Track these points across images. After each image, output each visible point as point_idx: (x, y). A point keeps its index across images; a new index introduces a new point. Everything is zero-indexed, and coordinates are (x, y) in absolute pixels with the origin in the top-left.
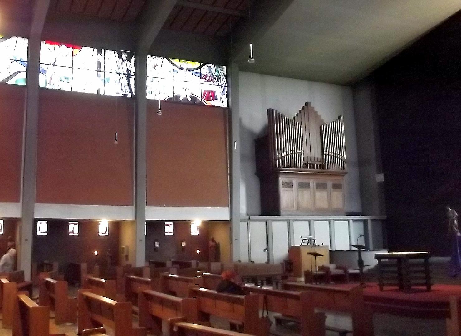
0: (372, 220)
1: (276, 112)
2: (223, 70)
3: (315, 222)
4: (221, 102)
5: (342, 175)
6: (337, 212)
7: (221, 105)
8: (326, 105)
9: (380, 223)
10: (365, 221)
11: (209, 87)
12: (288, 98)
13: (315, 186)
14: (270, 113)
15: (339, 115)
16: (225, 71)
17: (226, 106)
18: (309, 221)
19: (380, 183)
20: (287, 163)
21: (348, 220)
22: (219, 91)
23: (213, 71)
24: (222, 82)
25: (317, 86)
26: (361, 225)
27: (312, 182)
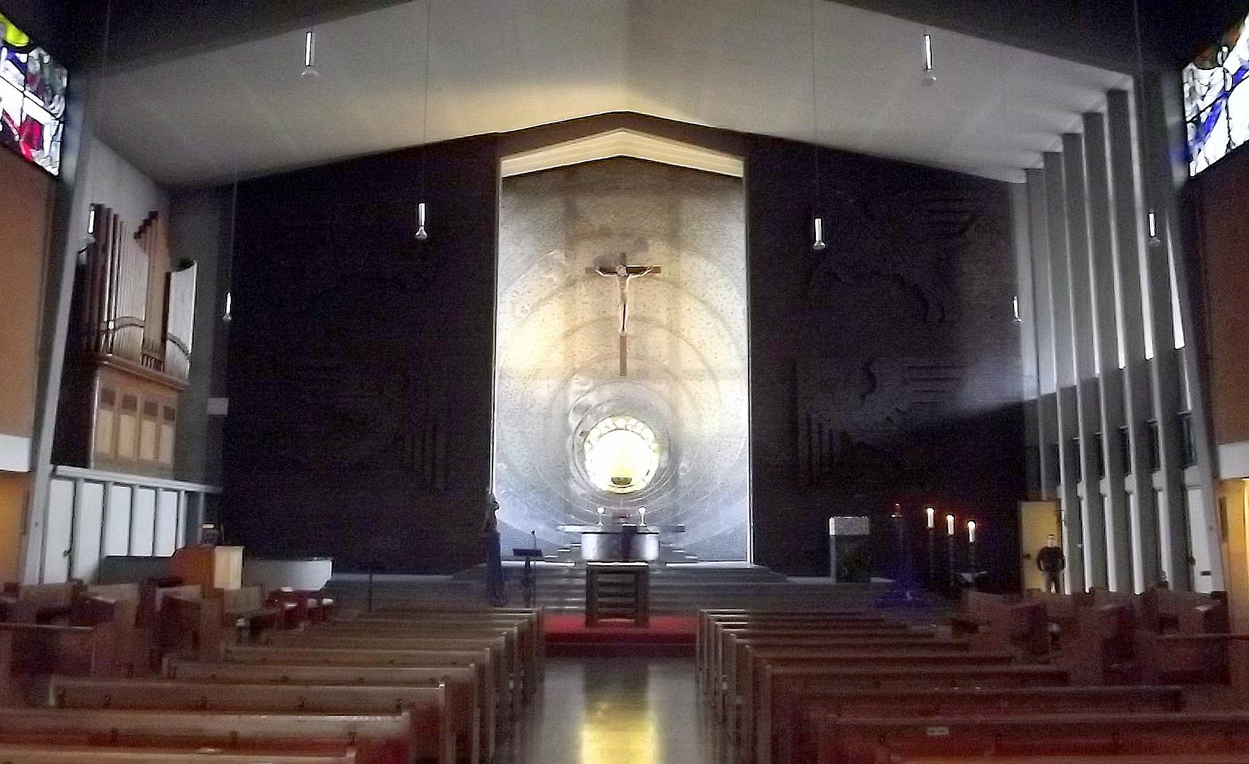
0: (207, 495)
1: (116, 217)
6: (160, 472)
7: (49, 169)
17: (55, 172)
19: (214, 418)
23: (47, 72)
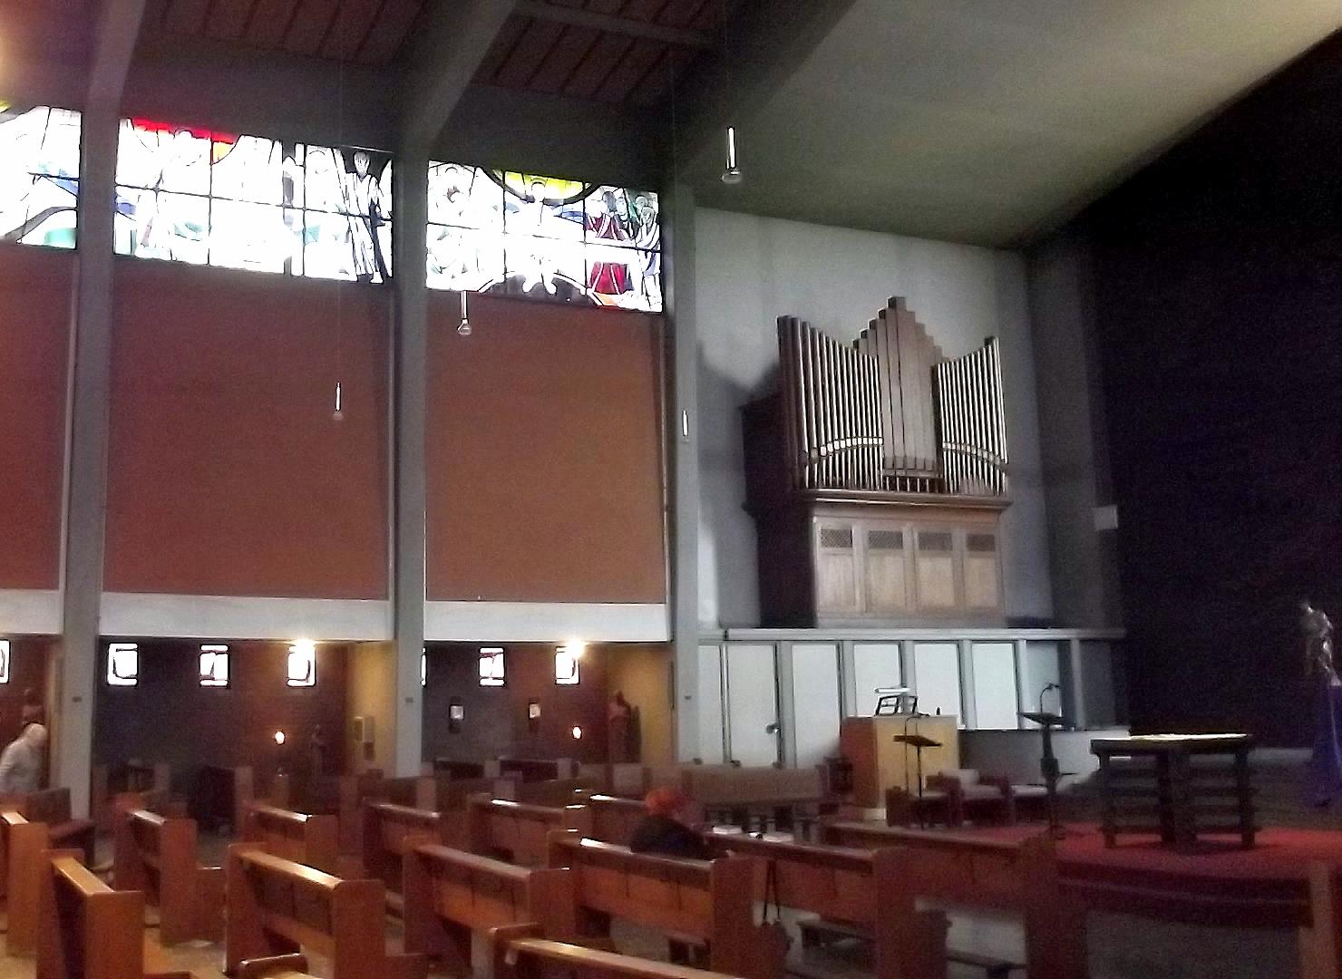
0: (1083, 641)
1: (804, 326)
2: (649, 205)
3: (918, 647)
4: (644, 297)
5: (996, 511)
6: (980, 618)
7: (644, 307)
8: (950, 306)
9: (1107, 649)
10: (1063, 645)
11: (608, 252)
12: (839, 285)
13: (917, 543)
14: (787, 328)
15: (988, 336)
16: (656, 206)
17: (658, 308)
18: (900, 643)
19: (1105, 534)
20: (834, 474)
21: (1014, 642)
22: (637, 265)
23: (621, 208)
24: (647, 239)
25: (923, 252)
26: (1051, 655)
27: (909, 531)
